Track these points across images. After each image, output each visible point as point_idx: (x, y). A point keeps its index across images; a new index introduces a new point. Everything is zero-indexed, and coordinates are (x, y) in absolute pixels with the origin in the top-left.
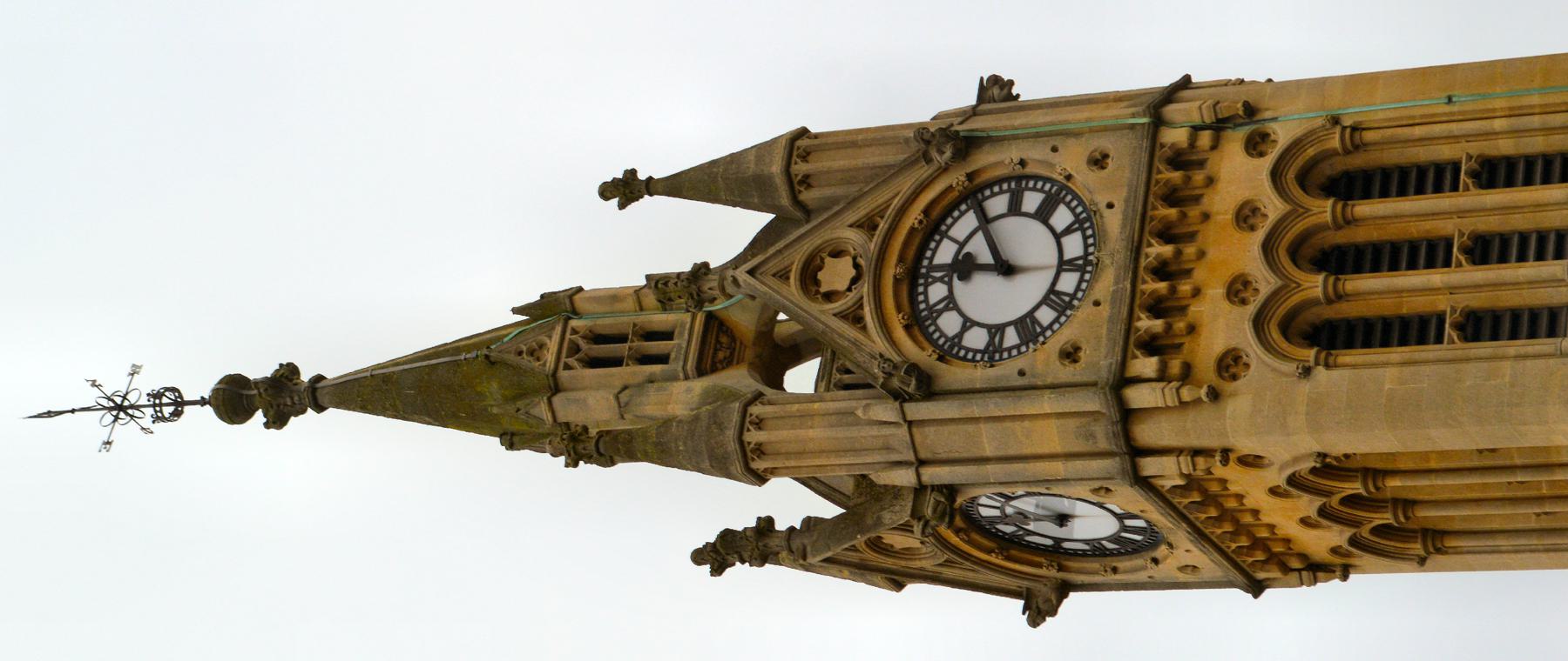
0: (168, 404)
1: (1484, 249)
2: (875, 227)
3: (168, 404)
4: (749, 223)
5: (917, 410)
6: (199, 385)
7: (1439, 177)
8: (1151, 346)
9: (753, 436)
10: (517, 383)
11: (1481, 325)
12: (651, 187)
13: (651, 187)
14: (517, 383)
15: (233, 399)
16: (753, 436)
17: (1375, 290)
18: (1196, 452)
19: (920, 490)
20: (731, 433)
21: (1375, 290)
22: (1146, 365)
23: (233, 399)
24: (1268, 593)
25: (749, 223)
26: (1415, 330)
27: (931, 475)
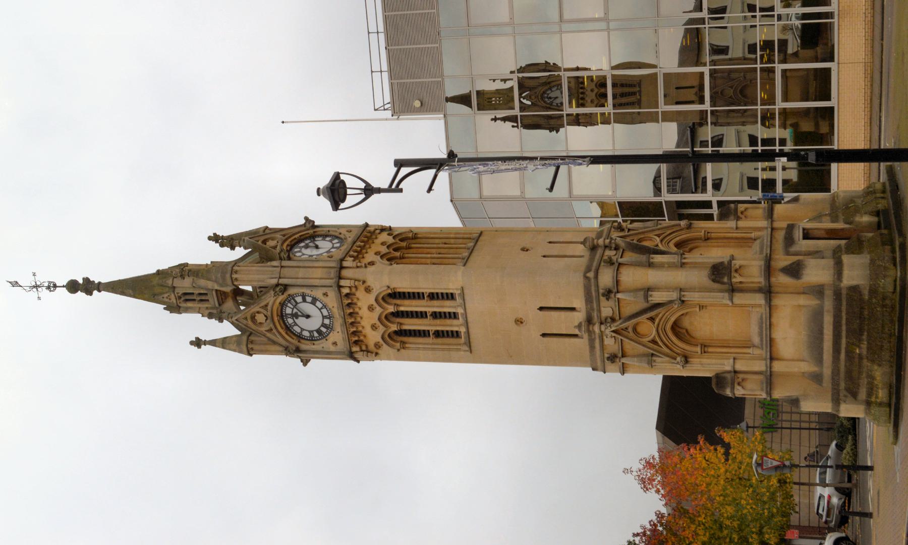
0: (52, 287)
1: (435, 315)
2: (604, 96)
3: (52, 287)
4: (257, 254)
5: (285, 263)
6: (27, 281)
8: (356, 342)
9: (234, 276)
10: (168, 288)
11: (438, 334)
12: (100, 287)
13: (100, 287)
14: (168, 288)
15: (73, 287)
16: (234, 276)
17: (410, 324)
18: (356, 280)
19: (277, 285)
20: (228, 276)
21: (410, 324)
23: (73, 287)
24: (313, 362)
25: (257, 254)
26: (424, 334)
27: (282, 281)
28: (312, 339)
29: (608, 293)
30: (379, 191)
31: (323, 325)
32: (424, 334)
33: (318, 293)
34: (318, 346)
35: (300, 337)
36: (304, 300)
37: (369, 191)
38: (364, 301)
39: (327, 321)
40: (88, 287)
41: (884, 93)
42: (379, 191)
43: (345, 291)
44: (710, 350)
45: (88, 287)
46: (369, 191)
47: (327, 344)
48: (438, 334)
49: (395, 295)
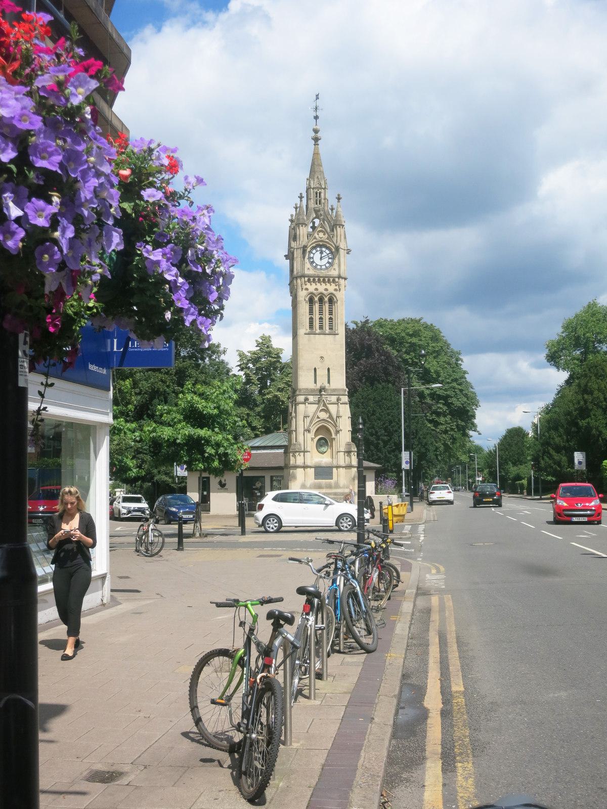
7: (331, 313)
8: (309, 281)
22: (306, 279)
29: (306, 399)
33: (336, 266)
38: (331, 288)
43: (337, 280)
47: (308, 265)
49: (331, 301)
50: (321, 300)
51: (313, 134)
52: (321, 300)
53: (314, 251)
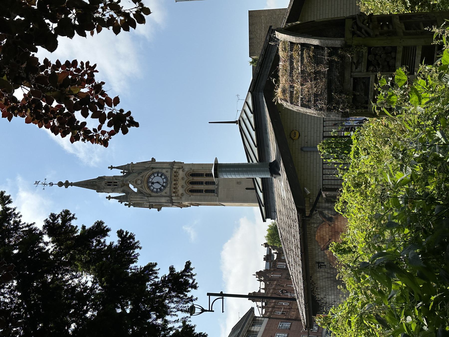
0: (51, 184)
3: (51, 184)
8: (174, 192)
11: (207, 191)
12: (72, 184)
13: (72, 184)
15: (60, 184)
17: (196, 187)
21: (196, 187)
22: (174, 195)
23: (60, 184)
28: (157, 192)
30: (206, 311)
31: (158, 176)
32: (200, 191)
33: (164, 171)
34: (159, 194)
35: (152, 191)
36: (161, 176)
37: (203, 310)
39: (160, 175)
40: (67, 184)
41: (413, 63)
42: (206, 311)
44: (174, 204)
45: (67, 184)
46: (203, 310)
48: (207, 191)
50: (192, 183)
51: (64, 186)
52: (192, 183)
53: (155, 190)
